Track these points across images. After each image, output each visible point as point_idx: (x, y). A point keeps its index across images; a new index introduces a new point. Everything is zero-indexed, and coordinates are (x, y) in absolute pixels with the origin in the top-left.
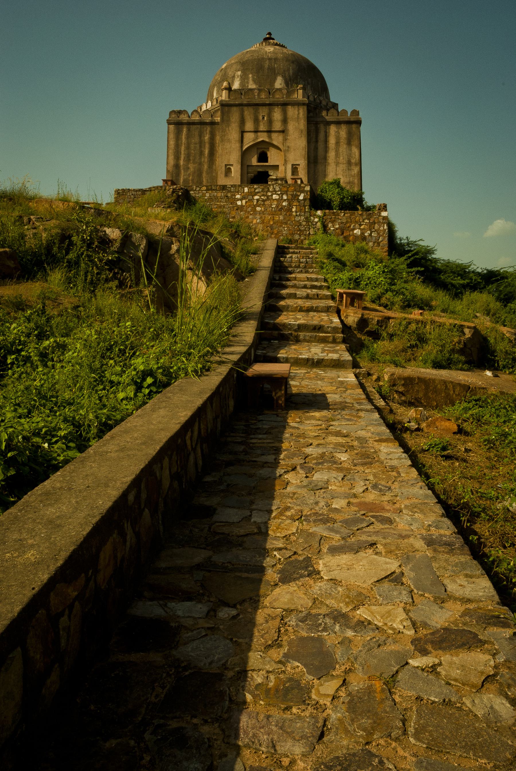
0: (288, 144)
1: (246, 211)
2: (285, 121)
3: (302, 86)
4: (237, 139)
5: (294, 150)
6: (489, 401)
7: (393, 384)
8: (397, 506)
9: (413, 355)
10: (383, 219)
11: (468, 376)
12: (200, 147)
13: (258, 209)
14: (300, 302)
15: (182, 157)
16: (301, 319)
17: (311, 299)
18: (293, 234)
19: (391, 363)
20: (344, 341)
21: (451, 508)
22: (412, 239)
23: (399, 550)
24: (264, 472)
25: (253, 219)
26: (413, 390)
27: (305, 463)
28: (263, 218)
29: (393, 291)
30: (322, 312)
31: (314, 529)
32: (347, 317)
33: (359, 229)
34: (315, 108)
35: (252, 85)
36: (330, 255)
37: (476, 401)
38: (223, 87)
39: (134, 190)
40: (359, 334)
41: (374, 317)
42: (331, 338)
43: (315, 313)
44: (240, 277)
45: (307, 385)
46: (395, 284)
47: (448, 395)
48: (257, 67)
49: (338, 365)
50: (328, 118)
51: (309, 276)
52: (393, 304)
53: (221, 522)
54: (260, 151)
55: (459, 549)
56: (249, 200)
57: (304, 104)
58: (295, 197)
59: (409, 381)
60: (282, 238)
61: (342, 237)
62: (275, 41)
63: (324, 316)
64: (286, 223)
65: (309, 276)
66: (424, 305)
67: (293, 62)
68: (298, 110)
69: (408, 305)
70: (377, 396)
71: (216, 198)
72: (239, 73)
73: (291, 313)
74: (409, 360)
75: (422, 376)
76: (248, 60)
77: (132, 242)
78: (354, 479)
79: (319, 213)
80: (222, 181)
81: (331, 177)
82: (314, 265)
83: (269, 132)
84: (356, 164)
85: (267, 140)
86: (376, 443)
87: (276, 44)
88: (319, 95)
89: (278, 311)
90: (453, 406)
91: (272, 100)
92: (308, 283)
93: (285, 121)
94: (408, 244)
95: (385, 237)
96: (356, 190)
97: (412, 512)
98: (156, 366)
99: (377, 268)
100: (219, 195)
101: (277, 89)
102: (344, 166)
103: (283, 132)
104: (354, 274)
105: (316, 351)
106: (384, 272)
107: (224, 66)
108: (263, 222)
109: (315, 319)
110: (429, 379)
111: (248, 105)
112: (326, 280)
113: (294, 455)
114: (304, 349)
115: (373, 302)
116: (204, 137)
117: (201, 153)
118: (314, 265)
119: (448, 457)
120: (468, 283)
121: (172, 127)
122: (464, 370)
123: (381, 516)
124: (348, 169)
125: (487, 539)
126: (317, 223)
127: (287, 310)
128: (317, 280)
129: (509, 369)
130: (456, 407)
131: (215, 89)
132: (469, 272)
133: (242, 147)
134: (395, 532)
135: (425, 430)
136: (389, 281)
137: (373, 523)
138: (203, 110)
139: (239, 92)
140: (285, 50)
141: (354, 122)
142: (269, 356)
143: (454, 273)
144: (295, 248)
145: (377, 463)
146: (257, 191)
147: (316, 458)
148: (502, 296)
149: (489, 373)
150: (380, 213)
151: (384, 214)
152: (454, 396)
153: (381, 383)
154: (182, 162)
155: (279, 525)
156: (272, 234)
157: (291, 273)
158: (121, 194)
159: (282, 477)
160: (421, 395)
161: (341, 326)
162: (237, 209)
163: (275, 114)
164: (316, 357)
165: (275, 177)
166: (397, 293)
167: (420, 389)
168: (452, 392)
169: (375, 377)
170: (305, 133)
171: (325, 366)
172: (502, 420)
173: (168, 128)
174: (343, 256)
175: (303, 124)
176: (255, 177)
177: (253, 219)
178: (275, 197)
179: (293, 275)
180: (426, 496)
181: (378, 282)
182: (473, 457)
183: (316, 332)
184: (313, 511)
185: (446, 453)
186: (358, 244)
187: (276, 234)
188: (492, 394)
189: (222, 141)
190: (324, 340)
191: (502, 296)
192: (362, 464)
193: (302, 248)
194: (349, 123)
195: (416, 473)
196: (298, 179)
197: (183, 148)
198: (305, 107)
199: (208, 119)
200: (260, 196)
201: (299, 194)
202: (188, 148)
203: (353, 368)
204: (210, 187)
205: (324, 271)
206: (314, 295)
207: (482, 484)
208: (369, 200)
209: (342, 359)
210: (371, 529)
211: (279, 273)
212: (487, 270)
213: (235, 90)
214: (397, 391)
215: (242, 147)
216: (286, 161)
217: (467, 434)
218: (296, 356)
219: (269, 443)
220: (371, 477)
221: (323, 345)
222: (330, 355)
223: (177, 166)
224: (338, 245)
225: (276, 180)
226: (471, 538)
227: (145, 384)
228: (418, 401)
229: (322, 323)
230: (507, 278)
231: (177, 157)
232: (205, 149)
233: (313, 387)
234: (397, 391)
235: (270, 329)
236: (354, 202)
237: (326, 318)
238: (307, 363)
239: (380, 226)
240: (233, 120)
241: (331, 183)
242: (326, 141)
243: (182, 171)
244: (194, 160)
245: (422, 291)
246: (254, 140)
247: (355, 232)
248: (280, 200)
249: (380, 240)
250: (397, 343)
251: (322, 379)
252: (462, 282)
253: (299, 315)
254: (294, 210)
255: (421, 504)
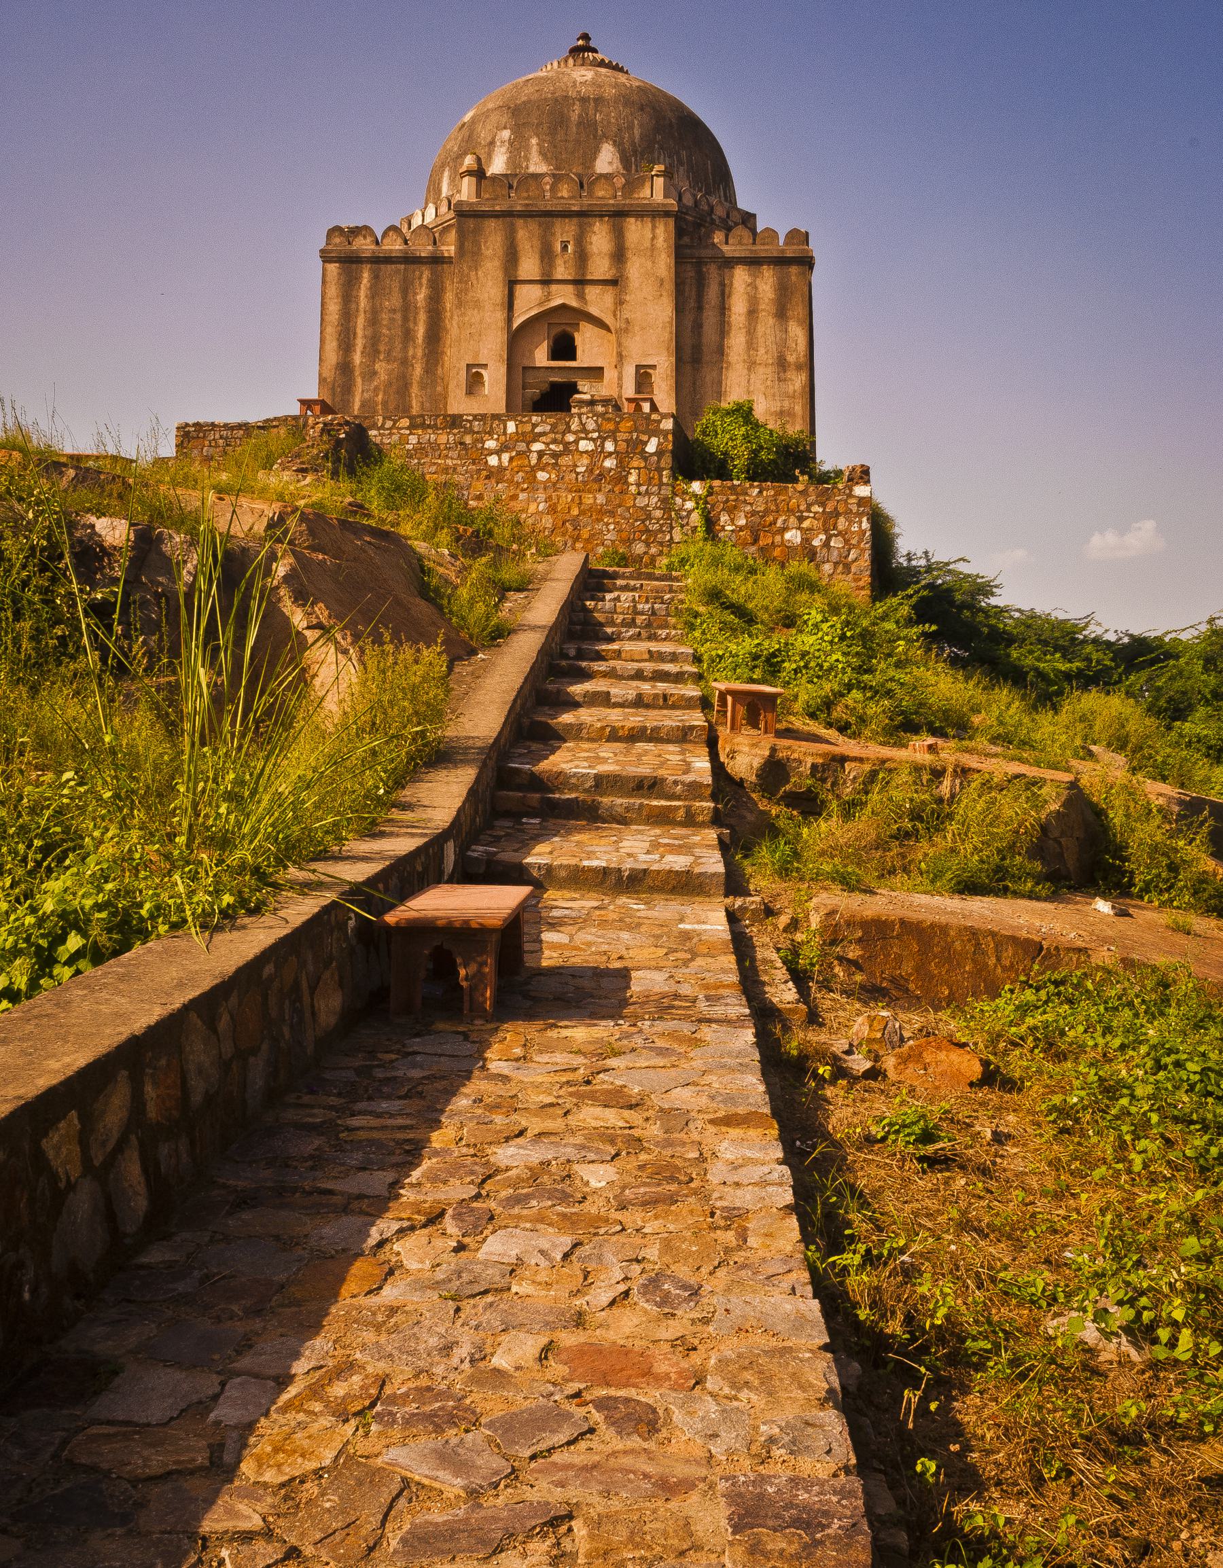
0: (626, 315)
1: (511, 481)
2: (619, 255)
3: (662, 168)
4: (499, 301)
5: (642, 329)
6: (1090, 986)
7: (833, 935)
8: (696, 1359)
9: (904, 857)
10: (859, 505)
11: (1042, 915)
12: (406, 319)
13: (542, 476)
14: (614, 716)
15: (360, 343)
16: (611, 760)
17: (647, 706)
18: (629, 542)
19: (834, 880)
20: (716, 820)
21: (889, 1348)
22: (939, 557)
23: (637, 1546)
24: (330, 1231)
25: (528, 501)
26: (887, 955)
27: (478, 1196)
28: (552, 500)
29: (864, 688)
30: (669, 741)
31: (394, 1454)
32: (732, 754)
33: (799, 528)
34: (698, 226)
35: (536, 165)
36: (714, 596)
37: (1057, 984)
38: (464, 169)
39: (226, 425)
40: (765, 801)
41: (804, 755)
42: (682, 812)
43: (650, 746)
44: (460, 650)
45: (589, 944)
46: (870, 671)
47: (980, 969)
48: (556, 122)
49: (685, 885)
50: (728, 250)
51: (654, 646)
52: (862, 720)
53: (109, 1423)
54: (556, 330)
55: (836, 1539)
56: (518, 453)
57: (667, 214)
58: (636, 447)
59: (876, 931)
60: (601, 550)
61: (753, 549)
62: (599, 56)
63: (672, 753)
64: (612, 514)
65: (654, 646)
66: (951, 725)
67: (642, 109)
68: (654, 228)
69: (906, 725)
70: (781, 973)
71: (435, 446)
72: (506, 134)
73: (586, 745)
74: (892, 872)
75: (913, 916)
76: (529, 101)
77: (162, 554)
78: (600, 1257)
79: (696, 487)
80: (458, 404)
81: (734, 394)
82: (672, 620)
83: (580, 283)
84: (799, 367)
85: (574, 303)
86: (712, 1129)
87: (602, 64)
88: (708, 193)
89: (551, 738)
90: (993, 999)
91: (586, 202)
92: (649, 667)
93: (619, 255)
94: (929, 569)
95: (863, 550)
96: (795, 429)
97: (733, 1385)
98: (88, 903)
99: (825, 626)
100: (443, 439)
101: (601, 175)
102: (770, 370)
103: (614, 282)
104: (766, 644)
105: (634, 848)
106: (843, 637)
107: (467, 117)
108: (552, 510)
109: (644, 761)
110: (932, 926)
111: (527, 215)
112: (697, 659)
113: (455, 1169)
114: (603, 841)
115: (812, 716)
116: (416, 294)
117: (408, 335)
118: (672, 620)
119: (933, 1162)
120: (1080, 670)
121: (333, 268)
122: (1038, 899)
123: (627, 1400)
124: (780, 380)
125: (988, 1453)
126: (690, 512)
127: (578, 738)
128: (674, 658)
129: (1161, 892)
130: (1000, 1002)
131: (446, 174)
132: (1085, 641)
133: (510, 320)
134: (649, 1469)
135: (892, 1075)
136: (855, 661)
137: (592, 1431)
138: (414, 227)
139: (506, 182)
140: (622, 78)
141: (795, 261)
142: (499, 862)
143: (1045, 643)
144: (631, 577)
145: (692, 1200)
146: (538, 430)
147: (515, 1184)
148: (1162, 703)
149: (1103, 906)
150: (851, 490)
151: (861, 491)
152: (999, 970)
153: (799, 937)
154: (357, 358)
155: (288, 1437)
156: (577, 539)
157: (610, 639)
158: (190, 435)
159: (387, 1247)
160: (907, 968)
161: (708, 780)
162: (487, 477)
163: (594, 239)
164: (628, 865)
165: (587, 397)
166: (876, 692)
167: (905, 953)
168: (992, 961)
169: (783, 920)
170: (670, 286)
171: (653, 889)
172: (1117, 1043)
173: (324, 270)
174: (750, 598)
175: (664, 264)
176: (544, 396)
177: (528, 501)
178: (584, 445)
179: (615, 646)
180: (799, 1323)
181: (826, 665)
182: (1014, 1159)
183: (643, 796)
184: (424, 1381)
185: (930, 1149)
186: (794, 567)
187: (587, 541)
188: (1098, 968)
189: (460, 304)
190: (662, 818)
191: (1162, 703)
192: (644, 1204)
193: (651, 577)
194: (780, 261)
195: (796, 1235)
196: (645, 400)
197: (361, 321)
198: (671, 222)
199: (425, 250)
200: (547, 444)
201: (645, 438)
202: (373, 321)
203: (726, 896)
204: (419, 420)
205: (697, 634)
206: (656, 696)
207: (1019, 1246)
208: (828, 456)
209: (697, 870)
210: (577, 1456)
211: (577, 638)
212: (1131, 636)
213: (495, 178)
214: (841, 959)
215: (510, 320)
216: (620, 356)
217: (1010, 1085)
218: (573, 861)
219: (401, 1128)
220: (652, 1253)
221: (658, 831)
222: (669, 858)
223: (345, 368)
224: (737, 569)
225: (592, 403)
226: (919, 1468)
227: (64, 952)
228: (899, 987)
229: (662, 773)
230: (1177, 657)
231: (346, 345)
232: (415, 323)
233: (605, 947)
234: (841, 959)
235: (519, 788)
236: (790, 461)
237: (675, 759)
238: (602, 883)
239: (851, 523)
240: (489, 252)
241: (728, 413)
242: (723, 309)
243: (359, 380)
244: (389, 353)
245: (944, 685)
246: (540, 304)
247: (788, 536)
248: (598, 454)
249: (852, 557)
250: (864, 825)
251: (634, 927)
252: (1064, 667)
253: (607, 750)
254: (632, 479)
255: (771, 1353)
